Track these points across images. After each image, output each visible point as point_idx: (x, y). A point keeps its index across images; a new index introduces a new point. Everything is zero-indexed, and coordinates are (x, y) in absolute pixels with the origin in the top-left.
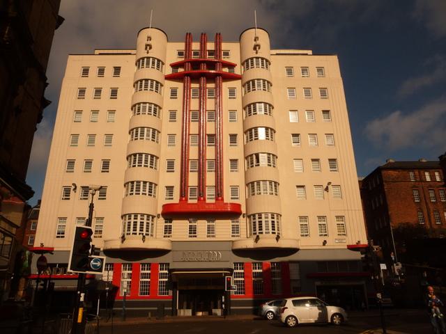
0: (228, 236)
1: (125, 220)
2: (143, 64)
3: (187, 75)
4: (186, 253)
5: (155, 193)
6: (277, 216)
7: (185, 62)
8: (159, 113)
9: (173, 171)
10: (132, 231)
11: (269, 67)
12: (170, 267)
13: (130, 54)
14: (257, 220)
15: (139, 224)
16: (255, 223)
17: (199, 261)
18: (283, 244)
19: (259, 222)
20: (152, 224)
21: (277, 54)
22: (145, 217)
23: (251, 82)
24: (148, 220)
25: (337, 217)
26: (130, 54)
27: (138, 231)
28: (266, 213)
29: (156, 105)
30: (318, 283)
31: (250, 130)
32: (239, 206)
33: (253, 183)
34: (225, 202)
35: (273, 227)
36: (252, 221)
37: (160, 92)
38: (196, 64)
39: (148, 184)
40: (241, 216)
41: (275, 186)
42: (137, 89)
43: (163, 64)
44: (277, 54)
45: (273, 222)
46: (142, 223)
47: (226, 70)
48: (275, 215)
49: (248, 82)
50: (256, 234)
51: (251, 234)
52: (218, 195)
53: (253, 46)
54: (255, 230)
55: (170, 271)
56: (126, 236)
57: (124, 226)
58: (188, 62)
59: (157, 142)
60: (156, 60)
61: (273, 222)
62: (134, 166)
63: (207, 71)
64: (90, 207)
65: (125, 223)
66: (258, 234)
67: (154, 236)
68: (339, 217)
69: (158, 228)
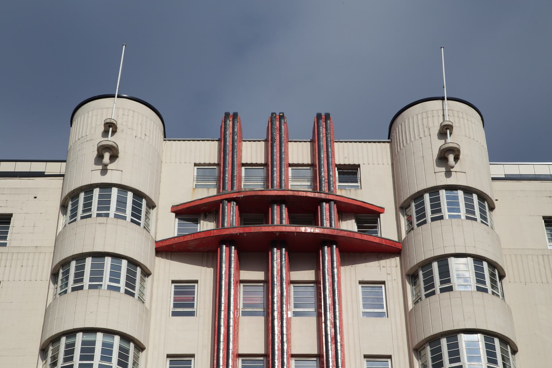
8: (147, 217)
9: (192, 314)
11: (491, 216)
13: (41, 175)
21: (508, 178)
26: (41, 175)
29: (126, 338)
37: (142, 293)
42: (74, 215)
43: (151, 205)
44: (508, 178)
49: (426, 264)
53: (436, 153)
60: (130, 195)
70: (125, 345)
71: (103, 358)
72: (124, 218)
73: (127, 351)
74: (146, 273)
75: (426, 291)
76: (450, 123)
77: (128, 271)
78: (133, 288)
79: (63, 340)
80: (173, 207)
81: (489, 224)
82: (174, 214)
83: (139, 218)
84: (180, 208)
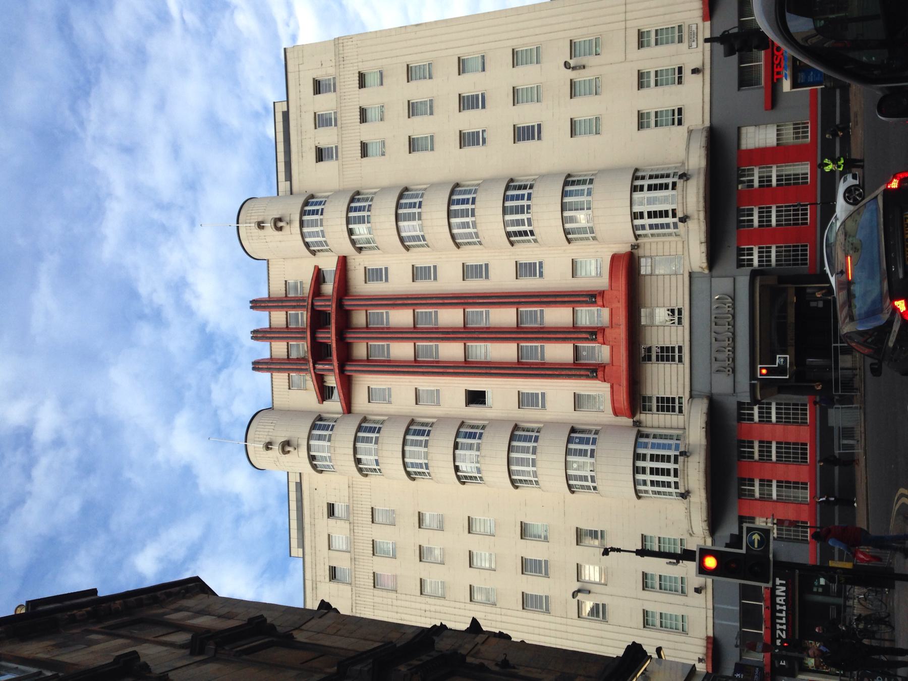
5: (589, 431)
12: (747, 400)
14: (646, 221)
15: (656, 465)
18: (697, 160)
20: (655, 437)
22: (640, 464)
25: (641, 45)
27: (671, 466)
30: (786, 85)
37: (371, 194)
38: (319, 352)
45: (650, 188)
55: (755, 401)
62: (532, 233)
66: (677, 453)
67: (680, 432)
68: (642, 40)
70: (412, 432)
71: (528, 452)
72: (330, 435)
73: (415, 430)
74: (365, 420)
75: (528, 236)
76: (273, 221)
77: (365, 431)
78: (375, 428)
79: (409, 469)
80: (319, 403)
81: (324, 200)
82: (324, 402)
83: (329, 425)
84: (320, 398)
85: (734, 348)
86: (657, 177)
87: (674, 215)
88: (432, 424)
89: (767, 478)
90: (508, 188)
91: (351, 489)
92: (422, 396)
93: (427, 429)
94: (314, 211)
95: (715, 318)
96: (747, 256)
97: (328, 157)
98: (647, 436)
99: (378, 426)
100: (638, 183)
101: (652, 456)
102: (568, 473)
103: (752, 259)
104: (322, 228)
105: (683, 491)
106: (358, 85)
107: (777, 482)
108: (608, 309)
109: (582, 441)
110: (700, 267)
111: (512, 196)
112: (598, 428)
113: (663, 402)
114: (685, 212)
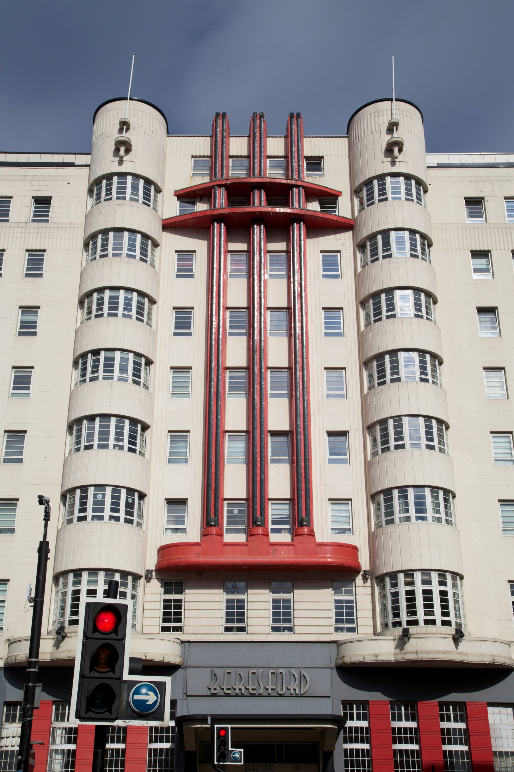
0: (262, 629)
1: (65, 585)
2: (109, 191)
3: (220, 219)
4: (219, 672)
5: (140, 516)
6: (454, 579)
7: (213, 187)
10: (421, 616)
13: (72, 165)
14: (402, 589)
16: (395, 595)
17: (253, 695)
19: (408, 593)
21: (440, 166)
22: (435, 577)
23: (380, 237)
24: (443, 583)
26: (72, 165)
28: (426, 572)
29: (142, 294)
31: (380, 357)
32: (354, 549)
33: (388, 492)
34: (319, 538)
35: (445, 608)
36: (389, 590)
37: (153, 260)
39: (124, 492)
40: (359, 580)
41: (446, 500)
43: (158, 190)
44: (440, 166)
46: (427, 593)
47: (314, 206)
48: (449, 577)
49: (373, 237)
50: (399, 624)
51: (385, 626)
52: (255, 523)
53: (384, 145)
54: (397, 615)
56: (68, 628)
57: (64, 601)
58: (220, 186)
59: (146, 387)
61: (443, 593)
63: (269, 209)
64: (40, 550)
65: (64, 594)
66: (404, 625)
69: (147, 614)
70: (141, 300)
72: (138, 201)
73: (143, 304)
79: (95, 295)
80: (175, 192)
82: (176, 198)
84: (181, 192)
85: (243, 696)
86: (456, 602)
87: (409, 623)
88: (149, 324)
89: (80, 737)
90: (134, 422)
91: (24, 225)
92: (333, 314)
93: (145, 318)
94: (411, 190)
95: (281, 673)
96: (357, 713)
97: (470, 212)
98: (134, 587)
99: (149, 259)
100: (449, 578)
101: (430, 592)
102: (89, 488)
103: (353, 720)
104: (128, 198)
105: (66, 630)
106: (474, 249)
107: (122, 749)
108: (199, 541)
109: (130, 506)
110: (344, 657)
111: (431, 427)
112: (144, 526)
113: (176, 607)
114: (415, 636)
